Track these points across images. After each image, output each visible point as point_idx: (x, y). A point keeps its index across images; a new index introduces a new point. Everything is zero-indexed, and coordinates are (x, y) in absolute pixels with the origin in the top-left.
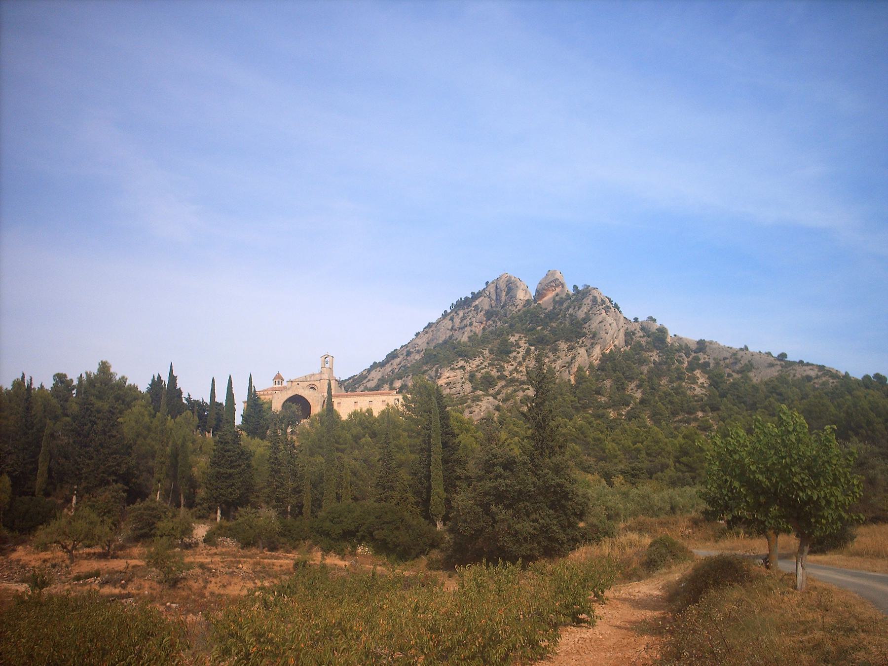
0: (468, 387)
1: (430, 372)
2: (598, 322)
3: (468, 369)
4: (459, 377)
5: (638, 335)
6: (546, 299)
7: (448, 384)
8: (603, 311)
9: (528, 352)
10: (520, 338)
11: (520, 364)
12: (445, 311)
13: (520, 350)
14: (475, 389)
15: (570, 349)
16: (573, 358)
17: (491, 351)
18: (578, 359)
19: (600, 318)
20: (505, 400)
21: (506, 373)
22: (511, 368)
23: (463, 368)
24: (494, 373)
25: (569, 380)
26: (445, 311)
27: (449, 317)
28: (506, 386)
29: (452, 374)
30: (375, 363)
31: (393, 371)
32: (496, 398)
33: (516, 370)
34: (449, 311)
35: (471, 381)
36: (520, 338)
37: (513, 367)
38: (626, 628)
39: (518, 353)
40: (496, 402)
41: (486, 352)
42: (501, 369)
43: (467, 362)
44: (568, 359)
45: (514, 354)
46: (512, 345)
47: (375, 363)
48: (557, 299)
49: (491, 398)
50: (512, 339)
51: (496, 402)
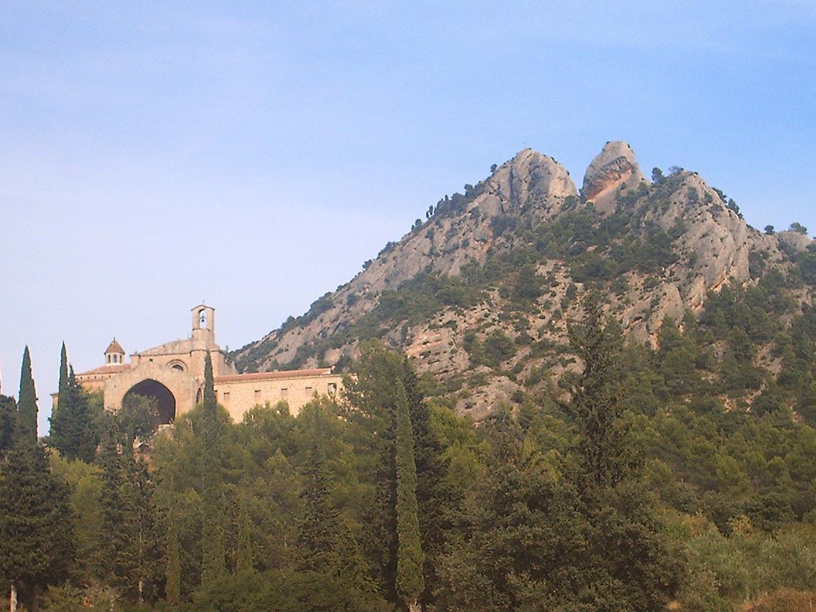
0: (462, 360)
1: (391, 333)
4: (445, 341)
5: (774, 257)
6: (602, 194)
7: (425, 354)
10: (557, 268)
12: (418, 221)
13: (557, 289)
14: (475, 363)
15: (649, 286)
16: (655, 302)
17: (504, 293)
18: (664, 303)
19: (703, 229)
20: (531, 383)
21: (532, 333)
22: (540, 323)
23: (452, 324)
24: (510, 333)
26: (418, 221)
27: (424, 232)
30: (291, 319)
32: (513, 379)
33: (550, 326)
35: (467, 349)
36: (557, 268)
39: (554, 295)
41: (495, 295)
42: (522, 326)
43: (460, 313)
44: (646, 304)
45: (546, 297)
46: (542, 280)
47: (291, 319)
48: (624, 193)
50: (542, 270)
51: (515, 387)
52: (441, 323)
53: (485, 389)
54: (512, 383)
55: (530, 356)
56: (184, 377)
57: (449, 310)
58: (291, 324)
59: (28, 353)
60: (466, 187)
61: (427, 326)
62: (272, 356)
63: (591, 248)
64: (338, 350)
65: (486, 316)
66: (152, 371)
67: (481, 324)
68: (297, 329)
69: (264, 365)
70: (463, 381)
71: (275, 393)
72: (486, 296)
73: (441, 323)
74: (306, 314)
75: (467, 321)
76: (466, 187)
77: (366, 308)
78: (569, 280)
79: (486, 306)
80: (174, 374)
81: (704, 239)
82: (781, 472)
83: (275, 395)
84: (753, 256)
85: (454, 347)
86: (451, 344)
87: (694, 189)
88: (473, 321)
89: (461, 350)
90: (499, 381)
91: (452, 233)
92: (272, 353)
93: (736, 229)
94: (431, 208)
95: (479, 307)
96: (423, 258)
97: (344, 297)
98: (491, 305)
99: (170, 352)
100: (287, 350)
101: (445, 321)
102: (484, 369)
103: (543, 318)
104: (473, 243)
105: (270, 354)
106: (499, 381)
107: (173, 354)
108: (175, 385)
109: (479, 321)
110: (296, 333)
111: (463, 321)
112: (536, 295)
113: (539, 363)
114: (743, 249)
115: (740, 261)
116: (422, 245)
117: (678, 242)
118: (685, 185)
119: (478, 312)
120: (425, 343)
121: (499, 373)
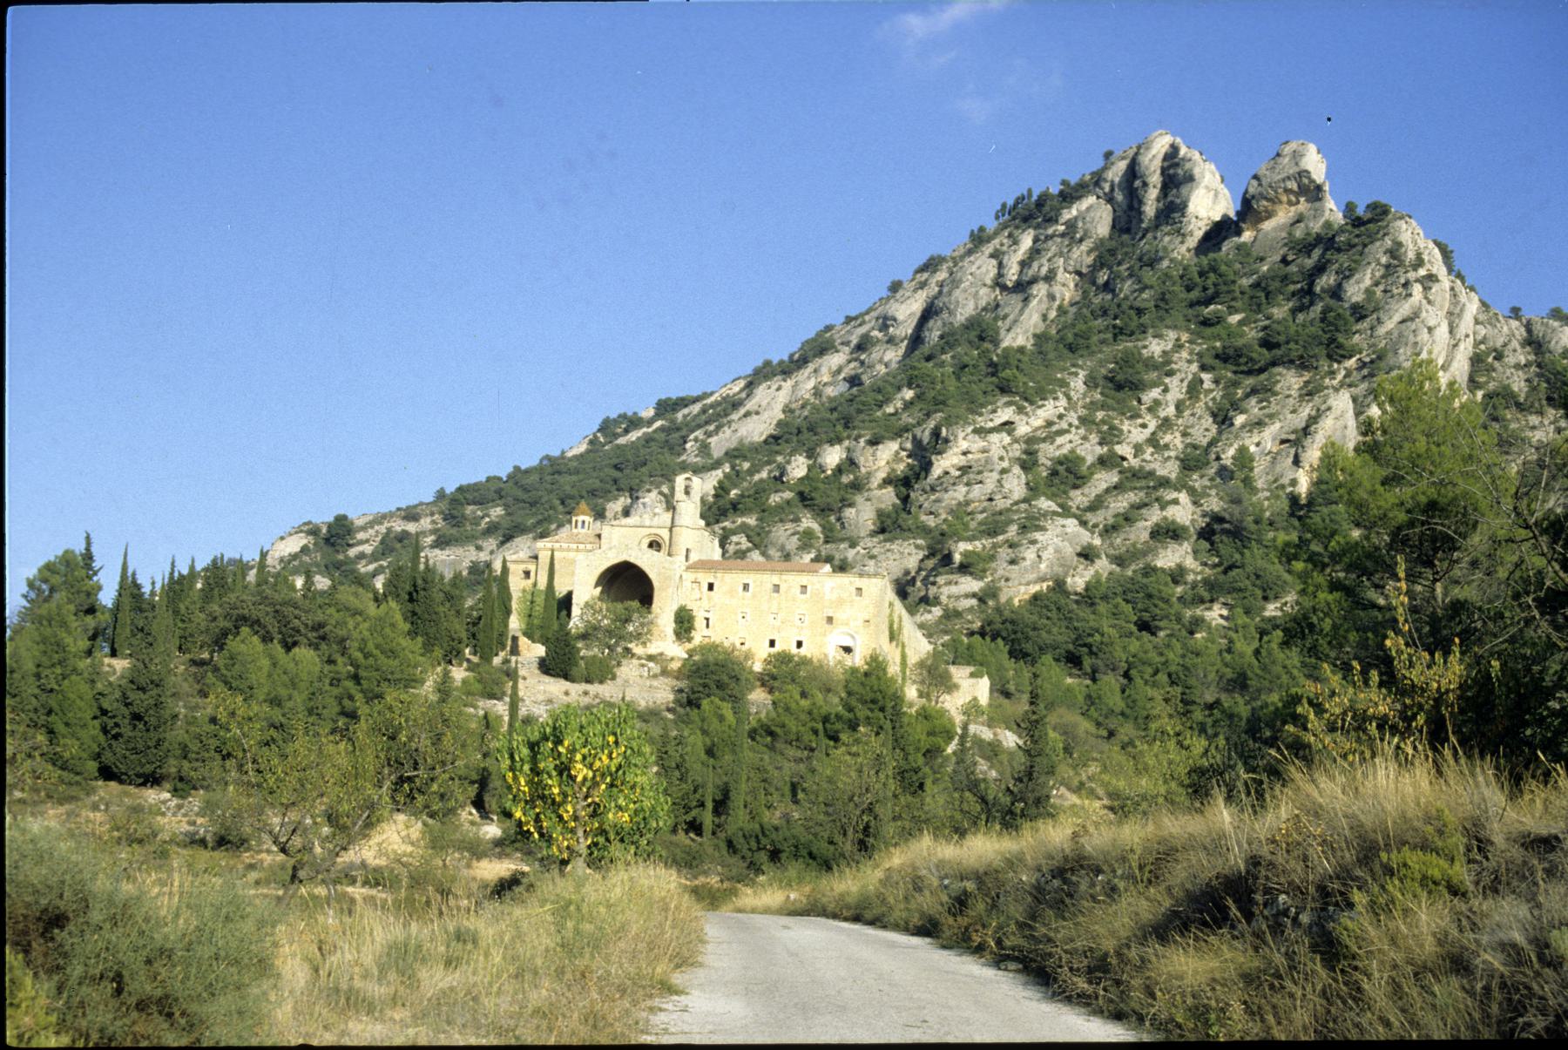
0: (1016, 485)
1: (918, 431)
2: (1397, 318)
3: (1022, 429)
4: (996, 452)
5: (1511, 360)
6: (1267, 226)
7: (965, 470)
8: (1417, 289)
9: (1194, 388)
10: (1178, 346)
11: (1166, 424)
12: (982, 229)
13: (1172, 382)
14: (1033, 490)
15: (1309, 392)
16: (1313, 420)
17: (1091, 383)
18: (1327, 426)
19: (1405, 309)
20: (1109, 530)
21: (1123, 449)
22: (1139, 435)
23: (1008, 426)
24: (1090, 451)
25: (1294, 482)
26: (982, 229)
27: (989, 249)
28: (1117, 488)
29: (977, 443)
30: (768, 363)
31: (817, 392)
32: (1083, 523)
33: (1153, 441)
34: (991, 225)
35: (1025, 467)
36: (1178, 346)
37: (1147, 432)
38: (172, 573)
39: (1166, 390)
40: (1085, 537)
41: (1078, 384)
42: (1110, 436)
43: (1021, 410)
44: (1299, 420)
45: (1155, 393)
46: (1150, 364)
47: (768, 363)
48: (1299, 233)
49: (1071, 524)
50: (1155, 347)
51: (1085, 537)
53: (1038, 535)
54: (1082, 530)
55: (1115, 487)
60: (1064, 183)
61: (970, 429)
63: (1234, 319)
64: (837, 447)
67: (1051, 431)
68: (776, 382)
74: (791, 356)
76: (1064, 183)
77: (886, 359)
78: (1194, 367)
79: (1063, 402)
81: (1403, 326)
82: (53, 1018)
84: (1476, 360)
86: (1001, 459)
87: (1400, 244)
89: (1017, 470)
91: (1035, 252)
93: (1457, 311)
94: (1004, 205)
96: (983, 291)
100: (757, 413)
101: (998, 421)
102: (1045, 504)
103: (1144, 426)
104: (1061, 276)
109: (1049, 424)
110: (775, 387)
112: (1136, 387)
113: (1132, 497)
114: (1462, 346)
115: (1455, 365)
116: (984, 269)
117: (1365, 324)
120: (965, 454)
121: (1066, 512)
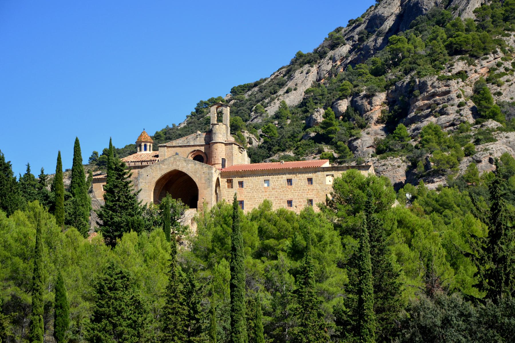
23: (462, 75)
30: (300, 55)
47: (300, 55)
52: (450, 74)
56: (205, 169)
57: (458, 60)
58: (302, 60)
59: (79, 145)
62: (280, 95)
65: (499, 65)
66: (178, 163)
69: (272, 104)
70: (469, 137)
71: (282, 182)
72: (500, 43)
73: (450, 74)
75: (478, 71)
80: (197, 166)
83: (281, 184)
85: (462, 99)
88: (484, 71)
90: (507, 137)
92: (281, 92)
95: (491, 57)
97: (355, 33)
98: (504, 52)
99: (192, 144)
100: (295, 89)
101: (454, 72)
105: (279, 94)
106: (507, 137)
107: (193, 146)
108: (198, 175)
111: (473, 71)
118: (475, 275)
119: (491, 60)
